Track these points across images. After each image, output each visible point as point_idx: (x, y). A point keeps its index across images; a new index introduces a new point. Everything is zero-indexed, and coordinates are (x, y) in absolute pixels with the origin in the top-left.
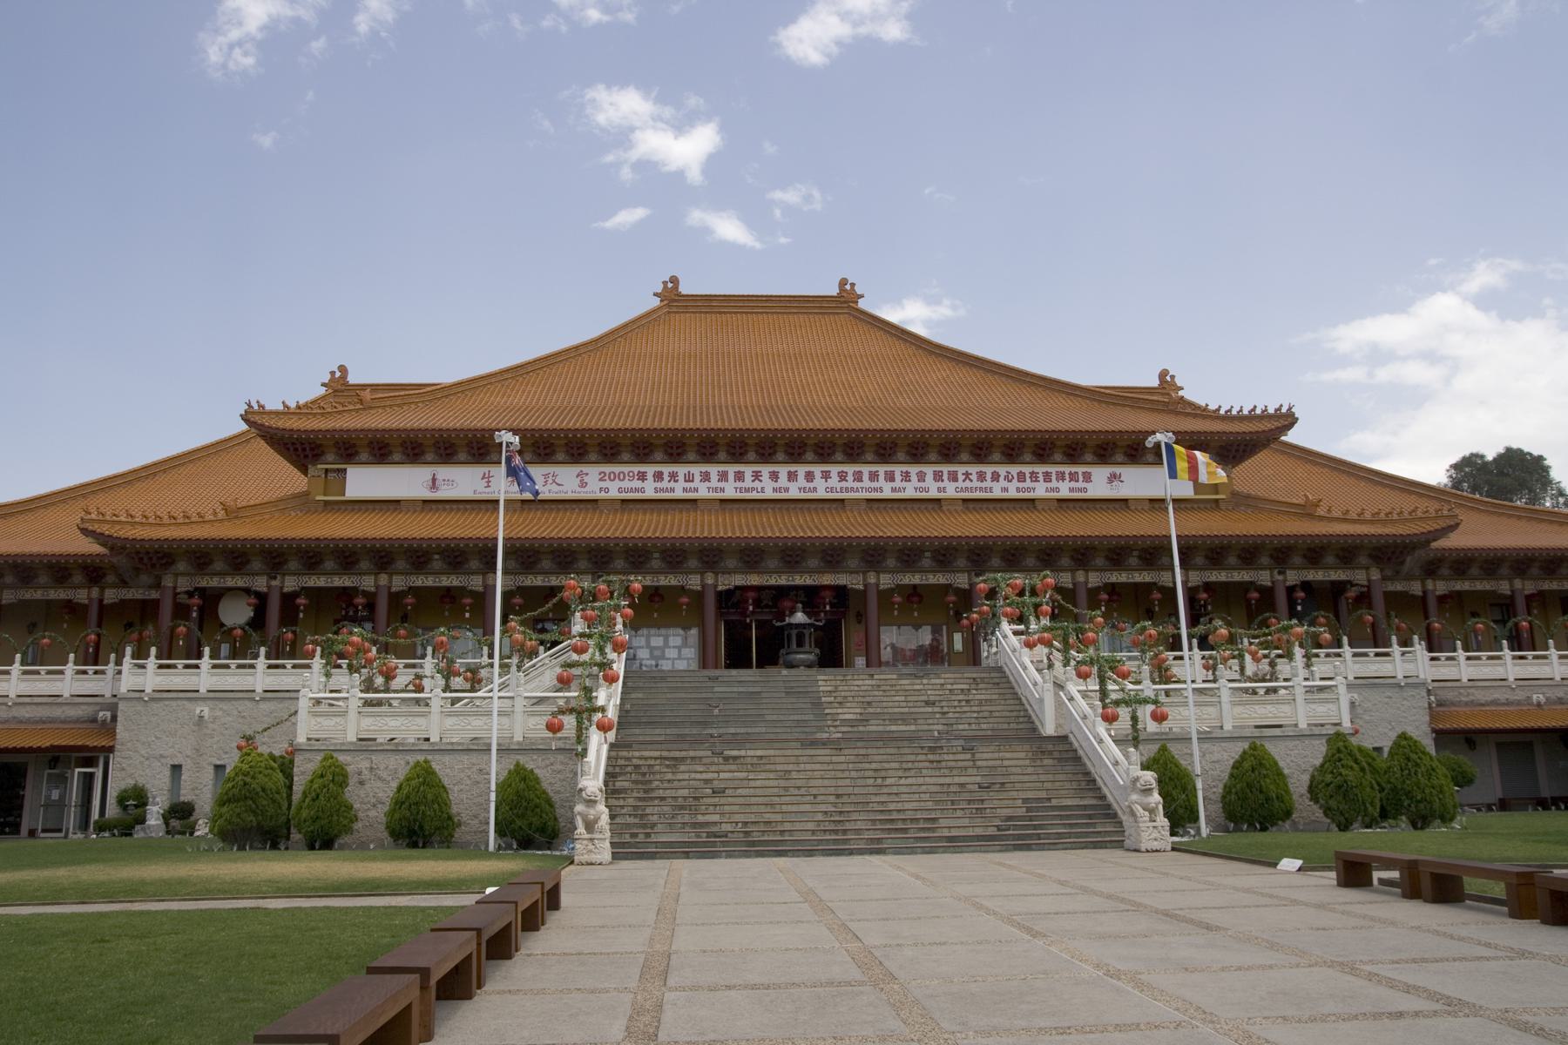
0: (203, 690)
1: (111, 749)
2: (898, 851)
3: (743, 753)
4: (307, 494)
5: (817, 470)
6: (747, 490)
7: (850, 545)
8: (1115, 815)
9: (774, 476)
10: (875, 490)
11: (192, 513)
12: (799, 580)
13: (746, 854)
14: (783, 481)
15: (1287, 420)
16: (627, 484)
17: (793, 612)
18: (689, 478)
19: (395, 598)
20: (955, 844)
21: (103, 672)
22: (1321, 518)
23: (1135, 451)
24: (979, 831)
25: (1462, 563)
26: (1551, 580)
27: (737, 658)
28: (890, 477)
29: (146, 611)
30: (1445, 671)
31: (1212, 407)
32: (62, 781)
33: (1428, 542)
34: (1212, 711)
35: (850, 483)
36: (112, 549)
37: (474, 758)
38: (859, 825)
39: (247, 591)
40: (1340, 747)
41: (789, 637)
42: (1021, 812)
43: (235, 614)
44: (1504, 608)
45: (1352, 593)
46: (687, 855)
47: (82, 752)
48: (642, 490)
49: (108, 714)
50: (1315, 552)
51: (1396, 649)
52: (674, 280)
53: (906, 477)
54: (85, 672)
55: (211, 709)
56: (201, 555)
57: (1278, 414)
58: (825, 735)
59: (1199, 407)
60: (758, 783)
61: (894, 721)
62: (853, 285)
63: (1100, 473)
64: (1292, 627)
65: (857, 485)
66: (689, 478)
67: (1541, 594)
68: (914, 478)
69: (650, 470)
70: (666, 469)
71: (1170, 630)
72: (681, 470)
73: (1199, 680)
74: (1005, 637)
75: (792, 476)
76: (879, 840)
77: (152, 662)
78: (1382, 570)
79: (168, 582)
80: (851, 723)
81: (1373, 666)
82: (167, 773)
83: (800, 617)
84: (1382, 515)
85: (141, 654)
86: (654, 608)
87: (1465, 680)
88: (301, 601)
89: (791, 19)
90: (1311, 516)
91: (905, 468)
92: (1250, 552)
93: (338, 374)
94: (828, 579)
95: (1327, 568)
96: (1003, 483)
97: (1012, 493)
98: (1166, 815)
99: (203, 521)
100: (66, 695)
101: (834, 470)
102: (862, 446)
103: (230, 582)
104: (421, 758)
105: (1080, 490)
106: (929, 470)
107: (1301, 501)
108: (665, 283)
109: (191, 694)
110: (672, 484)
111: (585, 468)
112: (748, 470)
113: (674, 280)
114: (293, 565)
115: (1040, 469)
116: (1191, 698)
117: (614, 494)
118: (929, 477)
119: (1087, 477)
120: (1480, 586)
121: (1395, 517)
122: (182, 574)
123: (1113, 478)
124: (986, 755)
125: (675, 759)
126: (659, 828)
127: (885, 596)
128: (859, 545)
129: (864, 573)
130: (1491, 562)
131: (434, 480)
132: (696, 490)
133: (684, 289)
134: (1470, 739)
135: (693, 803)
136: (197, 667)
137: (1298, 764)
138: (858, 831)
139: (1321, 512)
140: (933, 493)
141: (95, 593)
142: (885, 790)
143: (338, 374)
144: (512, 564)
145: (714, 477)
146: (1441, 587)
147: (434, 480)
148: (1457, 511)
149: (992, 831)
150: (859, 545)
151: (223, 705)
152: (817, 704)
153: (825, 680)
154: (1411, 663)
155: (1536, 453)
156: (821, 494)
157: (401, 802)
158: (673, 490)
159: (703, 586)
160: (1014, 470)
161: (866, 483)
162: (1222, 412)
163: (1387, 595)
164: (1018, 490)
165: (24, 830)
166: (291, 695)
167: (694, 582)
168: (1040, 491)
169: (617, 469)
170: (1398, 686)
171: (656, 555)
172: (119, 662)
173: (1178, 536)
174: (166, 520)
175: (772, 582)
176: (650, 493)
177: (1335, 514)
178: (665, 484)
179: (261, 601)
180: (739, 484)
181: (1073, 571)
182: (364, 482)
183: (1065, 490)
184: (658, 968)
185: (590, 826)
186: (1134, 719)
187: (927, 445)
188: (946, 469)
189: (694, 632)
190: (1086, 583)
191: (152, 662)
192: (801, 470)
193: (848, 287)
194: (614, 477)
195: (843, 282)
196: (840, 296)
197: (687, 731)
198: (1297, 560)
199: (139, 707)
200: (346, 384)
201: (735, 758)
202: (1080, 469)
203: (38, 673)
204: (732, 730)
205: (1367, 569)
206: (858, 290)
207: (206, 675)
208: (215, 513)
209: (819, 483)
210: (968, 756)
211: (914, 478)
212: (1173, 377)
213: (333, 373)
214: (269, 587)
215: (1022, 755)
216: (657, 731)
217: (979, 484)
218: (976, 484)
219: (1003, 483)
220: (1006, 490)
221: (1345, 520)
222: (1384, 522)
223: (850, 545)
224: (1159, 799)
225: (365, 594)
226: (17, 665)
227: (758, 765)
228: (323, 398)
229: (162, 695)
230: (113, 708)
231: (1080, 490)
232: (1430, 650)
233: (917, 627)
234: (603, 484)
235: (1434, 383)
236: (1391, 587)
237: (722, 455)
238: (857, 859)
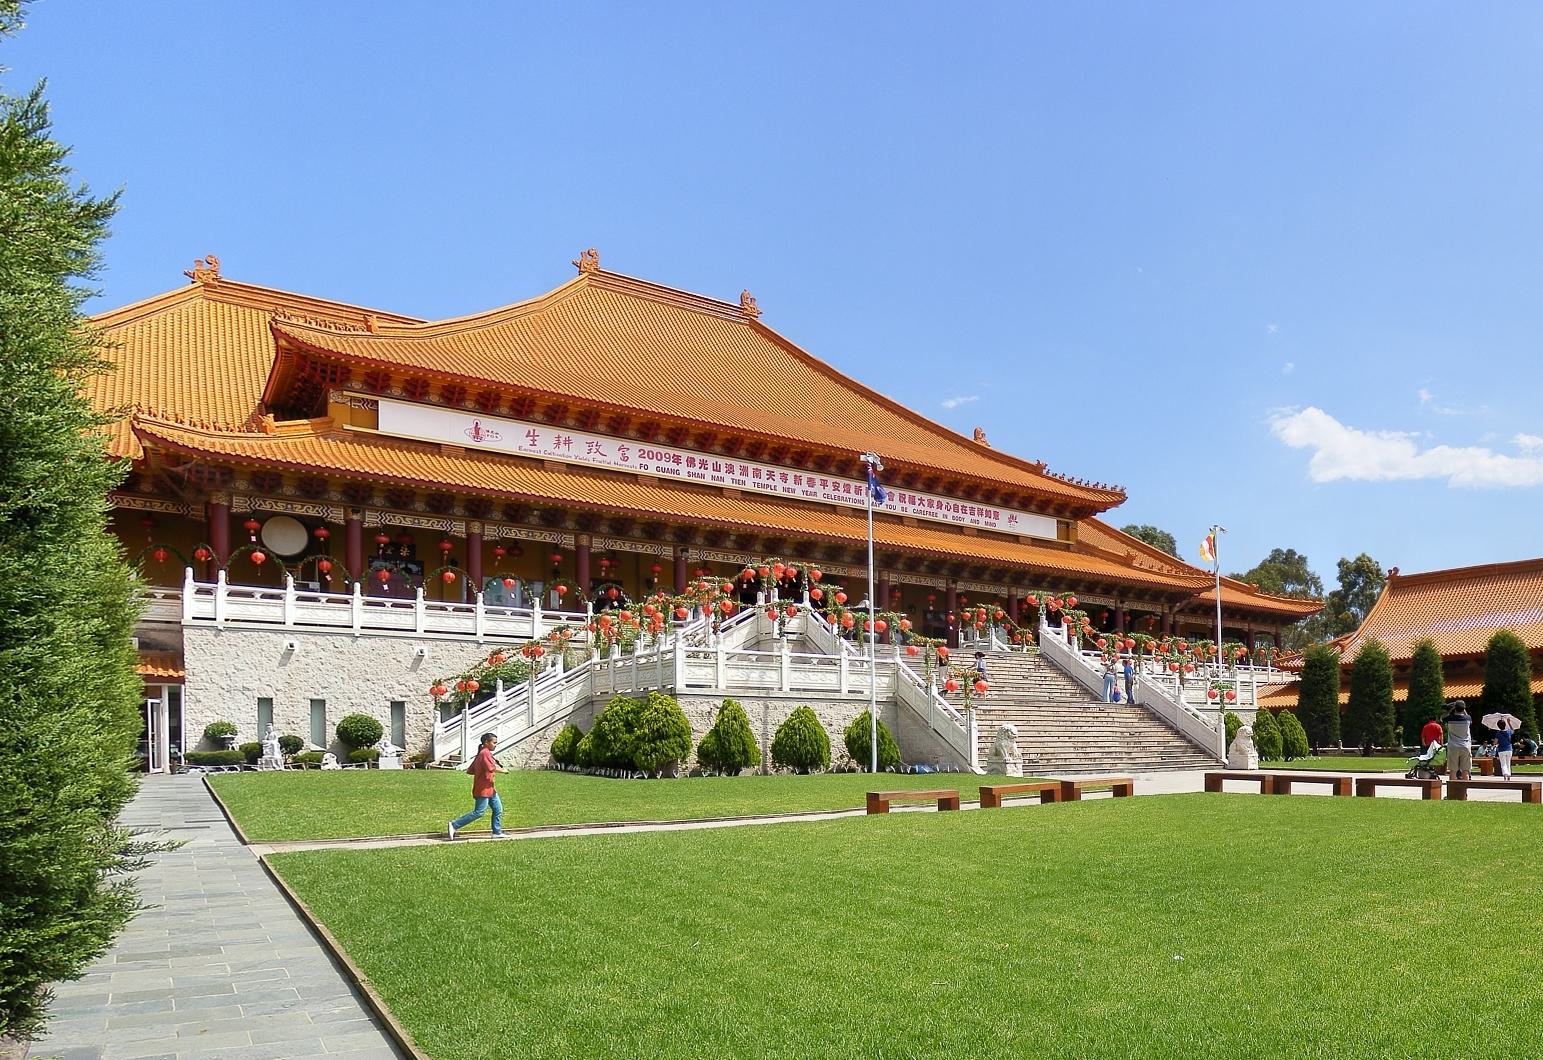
1: (182, 680)
6: (763, 486)
9: (784, 478)
10: (859, 502)
14: (790, 483)
16: (663, 464)
22: (1135, 568)
23: (357, 434)
35: (841, 494)
44: (461, 554)
48: (677, 472)
52: (1396, 570)
63: (1005, 514)
64: (35, 984)
65: (845, 495)
68: (804, 481)
71: (146, 755)
77: (222, 586)
84: (1100, 487)
85: (207, 575)
89: (1526, 434)
91: (744, 464)
95: (634, 540)
97: (949, 520)
104: (802, 705)
105: (991, 524)
109: (276, 626)
110: (702, 471)
111: (627, 444)
117: (652, 471)
119: (996, 516)
123: (1012, 519)
127: (489, 547)
131: (477, 429)
132: (722, 479)
137: (835, 723)
140: (898, 511)
145: (737, 471)
147: (477, 429)
155: (1267, 555)
156: (820, 498)
157: (789, 729)
158: (703, 476)
164: (713, 478)
168: (967, 521)
176: (683, 476)
178: (696, 470)
180: (757, 480)
182: (397, 418)
183: (982, 523)
187: (463, 391)
191: (222, 586)
194: (652, 456)
202: (993, 509)
203: (251, 595)
209: (818, 488)
211: (804, 481)
217: (929, 509)
218: (927, 509)
220: (945, 516)
226: (537, 608)
229: (237, 625)
231: (991, 524)
234: (644, 461)
235: (1364, 472)
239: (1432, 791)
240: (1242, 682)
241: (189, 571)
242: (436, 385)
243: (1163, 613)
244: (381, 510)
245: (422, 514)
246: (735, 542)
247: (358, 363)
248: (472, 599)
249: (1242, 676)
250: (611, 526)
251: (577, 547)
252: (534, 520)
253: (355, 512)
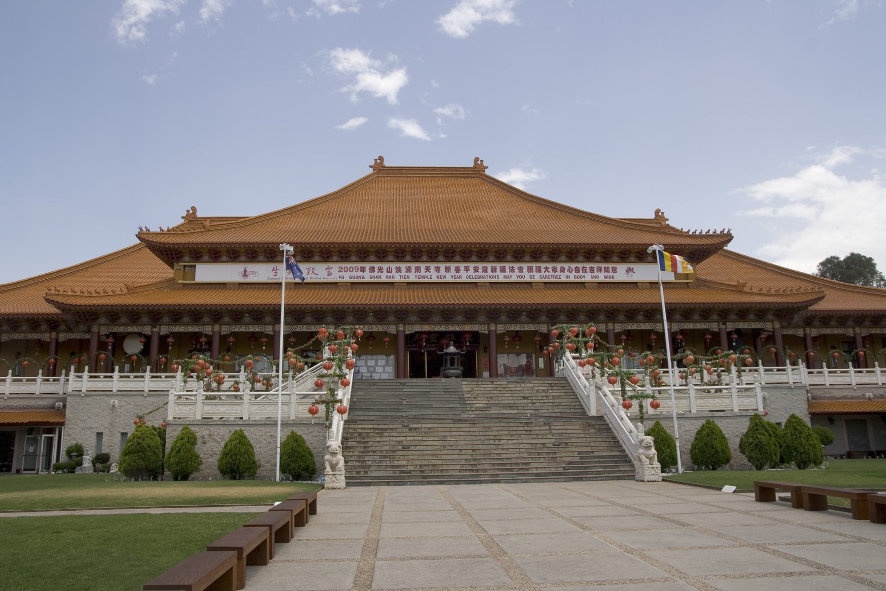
0: (115, 390)
1: (63, 424)
2: (507, 482)
3: (420, 426)
4: (173, 279)
5: (462, 266)
6: (422, 277)
7: (480, 308)
8: (630, 461)
9: (438, 269)
10: (495, 277)
11: (109, 290)
12: (451, 328)
13: (422, 483)
14: (442, 272)
15: (727, 237)
16: (354, 274)
17: (448, 346)
18: (389, 270)
19: (223, 338)
20: (540, 477)
21: (58, 380)
22: (747, 293)
23: (641, 255)
24: (553, 470)
25: (826, 318)
26: (876, 328)
27: (417, 372)
28: (503, 270)
29: (83, 345)
30: (816, 379)
31: (685, 230)
32: (35, 441)
33: (807, 307)
34: (685, 402)
35: (480, 273)
36: (63, 310)
37: (268, 429)
38: (486, 467)
39: (140, 334)
40: (757, 423)
41: (446, 360)
42: (577, 459)
43: (133, 347)
44: (850, 344)
45: (764, 335)
46: (388, 484)
47: (47, 425)
48: (363, 277)
49: (61, 404)
50: (743, 312)
51: (789, 367)
52: (381, 158)
53: (512, 270)
54: (48, 380)
55: (119, 401)
56: (113, 314)
57: (722, 234)
58: (466, 416)
59: (678, 230)
60: (428, 443)
61: (505, 408)
62: (482, 161)
63: (622, 268)
64: (730, 355)
65: (484, 274)
66: (389, 270)
67: (871, 336)
68: (516, 270)
69: (367, 266)
70: (377, 265)
71: (661, 356)
72: (385, 266)
73: (678, 385)
74: (568, 360)
75: (448, 269)
76: (497, 475)
77: (86, 374)
78: (781, 323)
79: (95, 329)
80: (481, 409)
81: (776, 377)
82: (95, 437)
83: (452, 349)
84: (781, 291)
85: (79, 370)
86: (369, 344)
87: (828, 385)
88: (170, 340)
89: (447, 11)
90: (741, 292)
91: (511, 265)
92: (706, 312)
93: (191, 212)
94: (468, 328)
95: (750, 321)
96: (567, 273)
97: (572, 279)
98: (659, 461)
99: (114, 295)
100: (37, 393)
101: (471, 266)
102: (487, 252)
103: (130, 329)
104: (238, 429)
105: (610, 277)
106: (525, 266)
107: (735, 283)
108: (376, 160)
109: (108, 393)
110: (380, 274)
111: (331, 265)
112: (423, 266)
113: (381, 158)
114: (166, 319)
115: (588, 265)
116: (673, 395)
117: (347, 279)
118: (525, 270)
119: (614, 270)
120: (836, 331)
121: (788, 292)
122: (103, 325)
123: (629, 270)
124: (557, 427)
125: (382, 429)
126: (373, 468)
127: (500, 337)
128: (485, 308)
129: (488, 324)
130: (843, 318)
131: (245, 271)
132: (393, 277)
133: (387, 164)
134: (830, 418)
135: (392, 454)
136: (111, 377)
137: (733, 432)
138: (485, 470)
139: (746, 289)
140: (527, 279)
141: (54, 335)
142: (500, 447)
143: (191, 212)
144: (289, 319)
145: (404, 270)
146: (814, 332)
147: (245, 271)
148: (823, 289)
149: (560, 470)
150: (485, 308)
151: (126, 399)
152: (462, 398)
153: (466, 385)
154: (797, 375)
155: (868, 256)
156: (464, 279)
157: (227, 453)
158: (380, 277)
159: (397, 332)
160: (573, 266)
161: (490, 273)
162: (691, 233)
163: (784, 336)
164: (575, 277)
165: (14, 470)
166: (165, 393)
167: (392, 329)
168: (588, 277)
169: (349, 265)
170: (790, 388)
171: (371, 314)
172: (67, 375)
173: (666, 303)
174: (94, 294)
175: (436, 329)
176: (367, 279)
177: (754, 291)
178: (376, 274)
179: (148, 340)
180: (417, 274)
181: (606, 323)
182: (206, 272)
183: (602, 277)
185: (333, 467)
186: (641, 407)
187: (524, 252)
188: (534, 265)
189: (392, 357)
190: (614, 329)
191: (86, 374)
192: (453, 266)
193: (479, 162)
194: (347, 270)
195: (476, 160)
196: (475, 167)
197: (388, 414)
198: (733, 317)
199: (79, 400)
200: (196, 217)
201: (415, 429)
202: (610, 265)
203: (21, 380)
204: (414, 413)
205: (773, 322)
206: (485, 164)
207: (116, 382)
208: (122, 290)
209: (463, 273)
210: (547, 428)
211: (516, 270)
212: (663, 213)
213: (188, 211)
214: (152, 332)
215: (578, 427)
216: (371, 414)
217: (553, 274)
218: (552, 274)
219: (567, 273)
220: (568, 277)
221: (760, 294)
222: (782, 295)
223: (480, 308)
224: (655, 452)
225: (206, 336)
226: (10, 376)
227: (428, 432)
228: (183, 225)
229: (91, 393)
230: (64, 401)
231: (610, 277)
232: (808, 367)
233: (518, 354)
234: (341, 274)
235: (810, 217)
236: (786, 332)
237: (408, 258)
238: (484, 486)
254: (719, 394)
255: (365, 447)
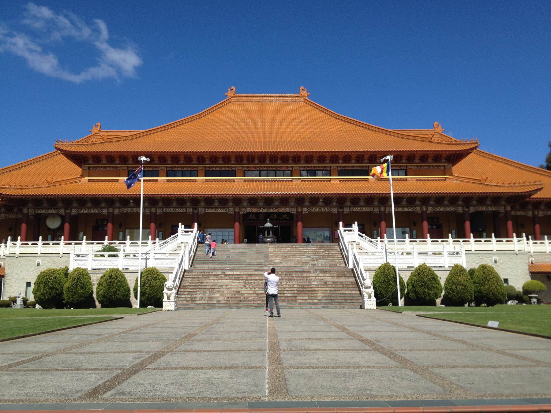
0: (39, 253)
3: (232, 273)
12: (271, 210)
29: (534, 220)
33: (531, 195)
40: (457, 270)
51: (515, 239)
55: (42, 260)
77: (19, 242)
79: (25, 211)
83: (268, 225)
85: (14, 239)
94: (282, 210)
95: (487, 206)
102: (312, 157)
114: (75, 205)
122: (116, 208)
125: (207, 275)
126: (197, 299)
129: (108, 209)
144: (147, 204)
151: (47, 259)
152: (267, 256)
171: (216, 201)
172: (6, 243)
175: (261, 211)
184: (274, 347)
185: (169, 298)
187: (402, 156)
190: (426, 211)
197: (216, 266)
199: (14, 260)
201: (229, 275)
207: (40, 247)
214: (65, 213)
216: (206, 266)
227: (237, 277)
239: (300, 388)
240: (420, 253)
241: (341, 223)
242: (303, 156)
243: (506, 211)
244: (308, 207)
245: (519, 210)
246: (406, 201)
247: (316, 154)
248: (125, 239)
249: (242, 361)
250: (420, 201)
251: (380, 212)
252: (489, 202)
253: (341, 208)
254: (128, 257)
255: (336, 285)
